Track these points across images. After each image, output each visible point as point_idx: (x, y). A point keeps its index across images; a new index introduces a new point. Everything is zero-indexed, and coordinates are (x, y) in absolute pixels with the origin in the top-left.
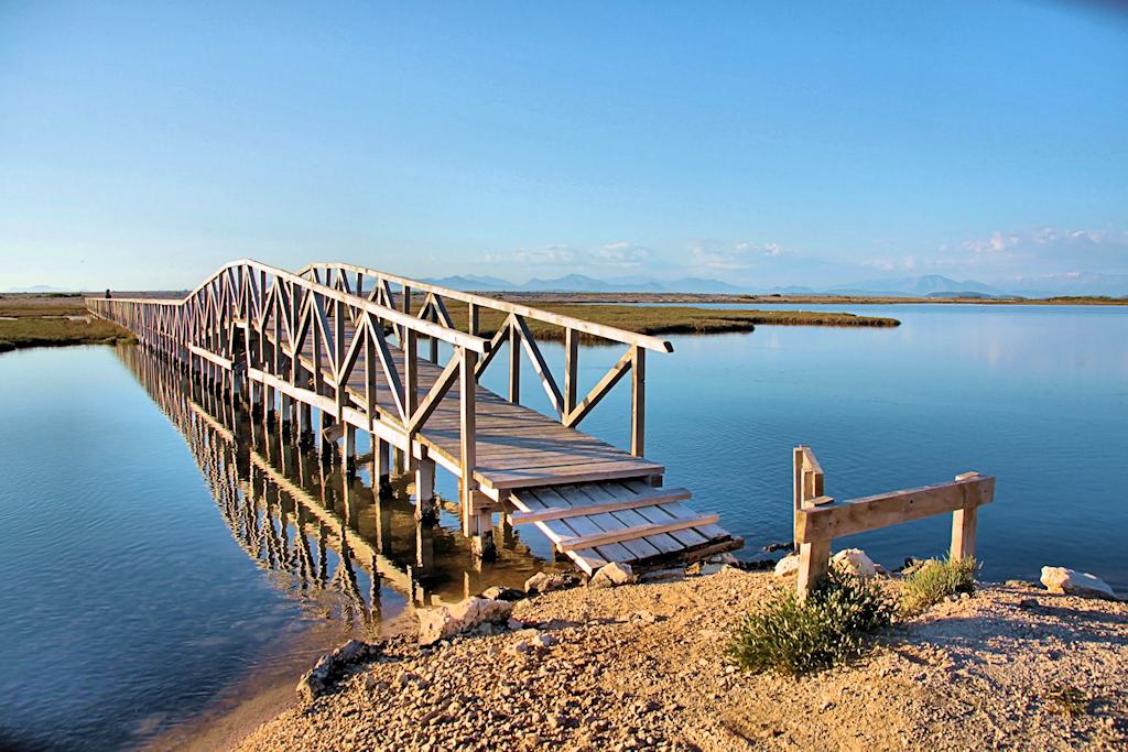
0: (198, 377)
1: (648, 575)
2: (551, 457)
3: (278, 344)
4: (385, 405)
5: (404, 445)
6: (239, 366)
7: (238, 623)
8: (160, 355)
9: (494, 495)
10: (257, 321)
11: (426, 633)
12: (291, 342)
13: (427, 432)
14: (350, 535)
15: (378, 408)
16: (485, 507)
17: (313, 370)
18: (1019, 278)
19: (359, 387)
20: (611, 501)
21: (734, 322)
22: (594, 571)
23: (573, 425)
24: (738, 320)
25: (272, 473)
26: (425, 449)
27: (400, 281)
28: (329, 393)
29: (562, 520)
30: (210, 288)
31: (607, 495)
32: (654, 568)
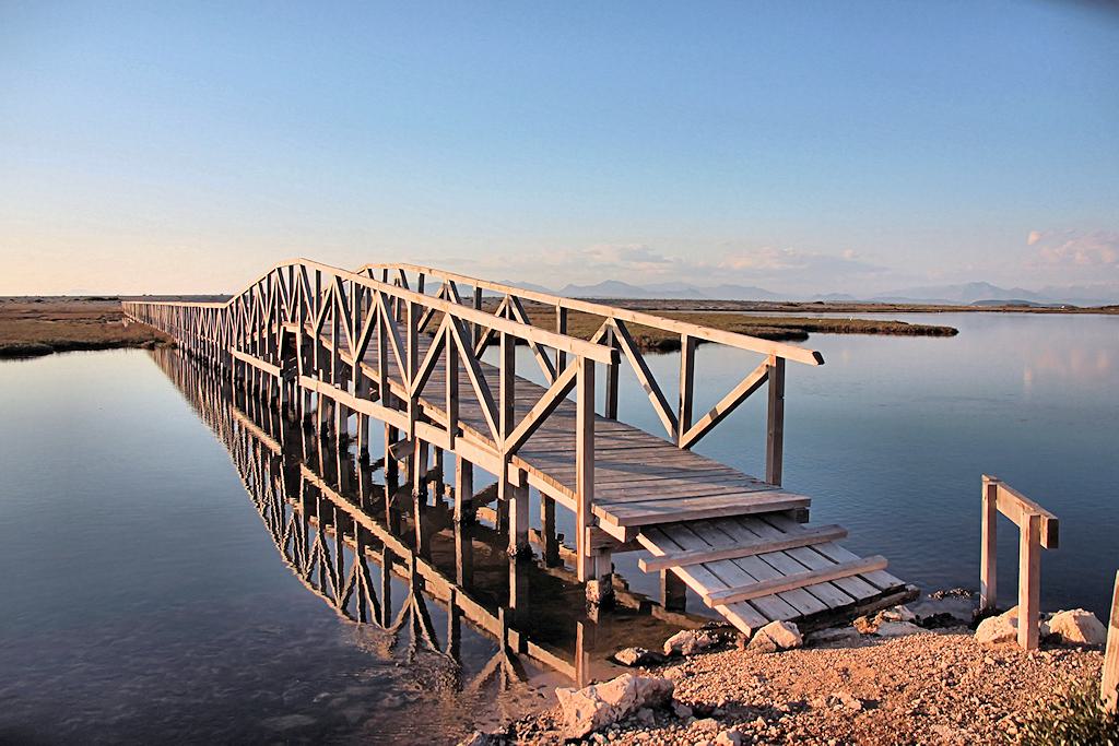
0: (241, 384)
1: (822, 635)
2: (678, 486)
3: (336, 350)
4: (469, 422)
5: (496, 467)
6: (289, 375)
7: (323, 695)
8: (203, 361)
9: (619, 533)
10: (310, 326)
11: (572, 723)
12: (352, 348)
13: (524, 456)
14: (424, 568)
15: (461, 425)
16: (604, 546)
17: (379, 380)
18: (1070, 285)
19: (436, 400)
20: (756, 542)
21: (787, 330)
22: (754, 631)
23: (687, 447)
24: (788, 327)
25: (326, 491)
26: (523, 475)
27: (495, 288)
28: (400, 405)
29: (702, 564)
30: (256, 290)
31: (747, 533)
32: (821, 626)
